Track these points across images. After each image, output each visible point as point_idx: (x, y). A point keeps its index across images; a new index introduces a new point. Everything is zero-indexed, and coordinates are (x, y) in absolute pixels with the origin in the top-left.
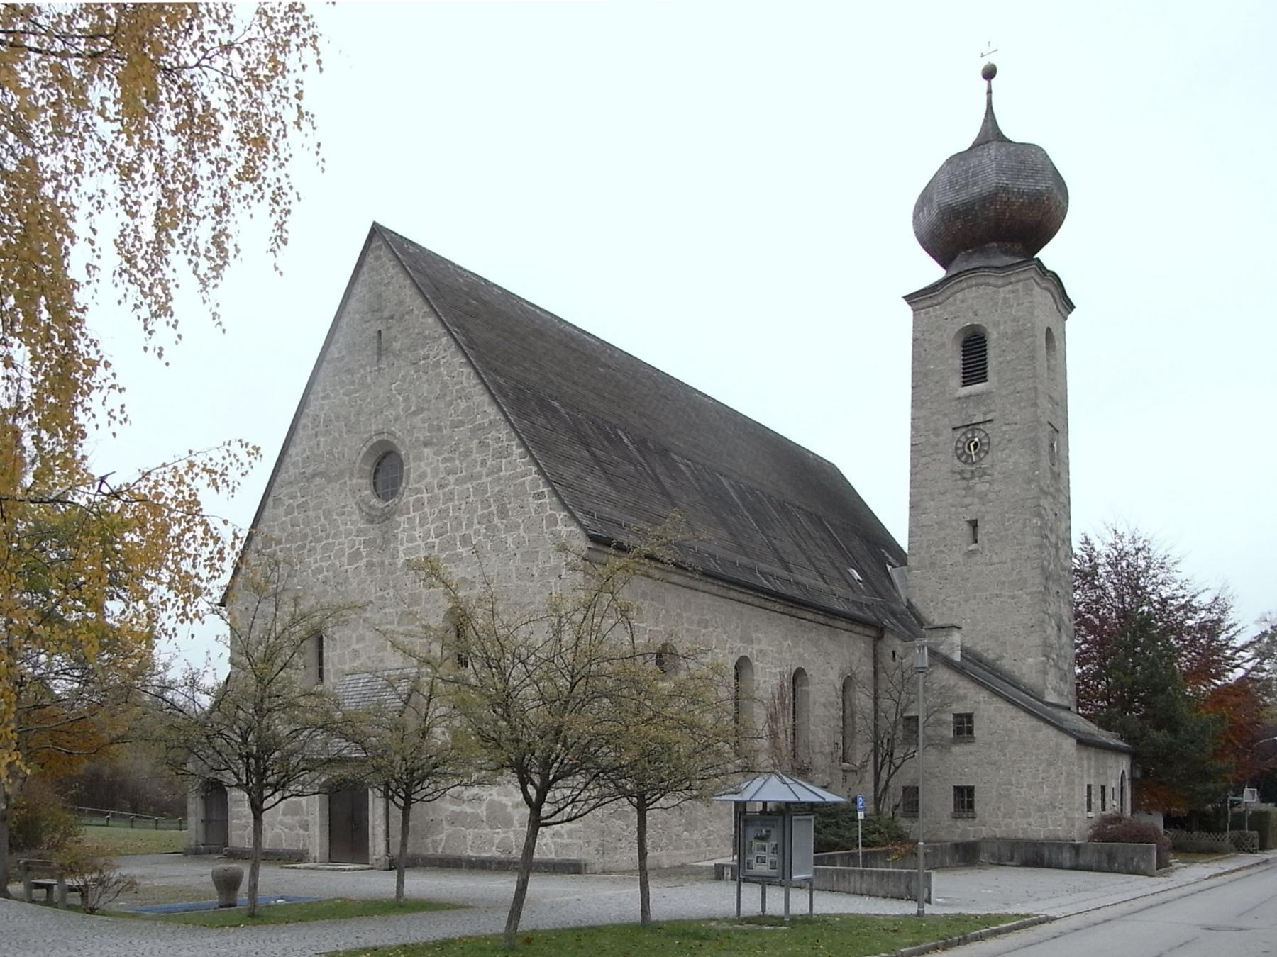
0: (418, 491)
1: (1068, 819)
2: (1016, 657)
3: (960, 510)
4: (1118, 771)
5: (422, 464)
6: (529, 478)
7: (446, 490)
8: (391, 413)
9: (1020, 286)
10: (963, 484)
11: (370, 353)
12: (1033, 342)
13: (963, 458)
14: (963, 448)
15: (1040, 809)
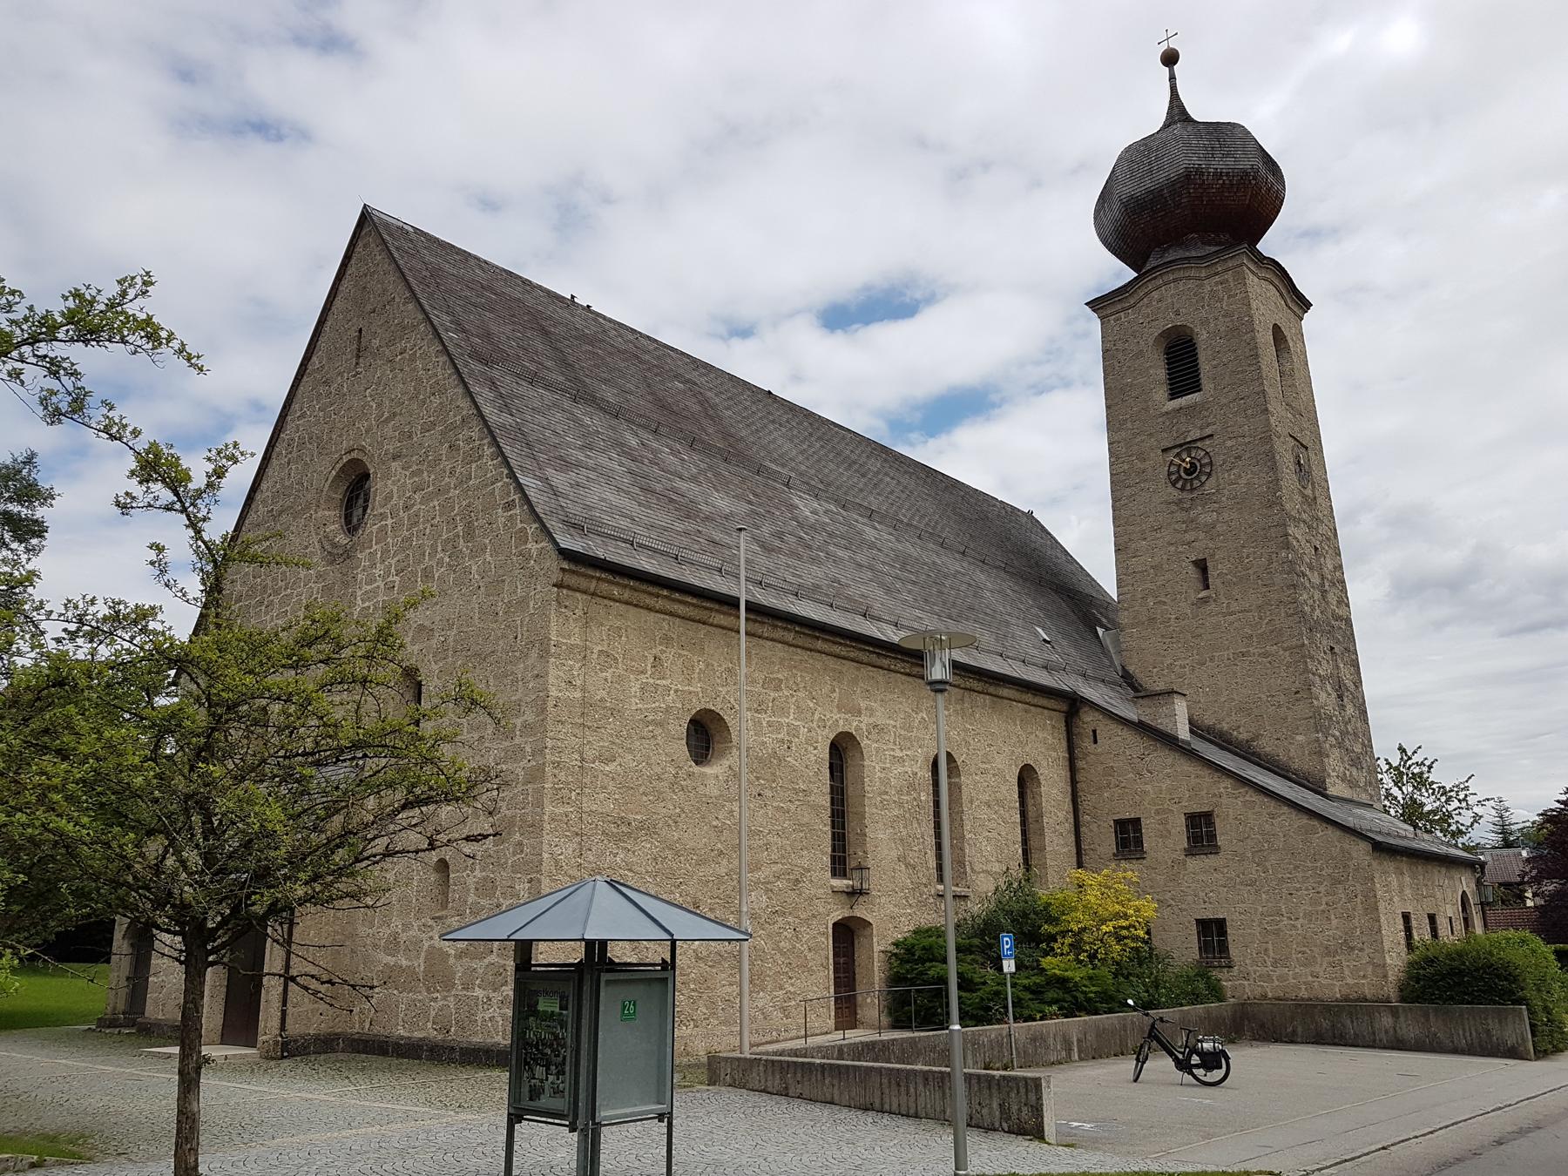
1: (1376, 966)
4: (1455, 891)
6: (499, 484)
8: (362, 425)
9: (1229, 276)
10: (1180, 516)
12: (1253, 338)
13: (1179, 485)
15: (1328, 952)
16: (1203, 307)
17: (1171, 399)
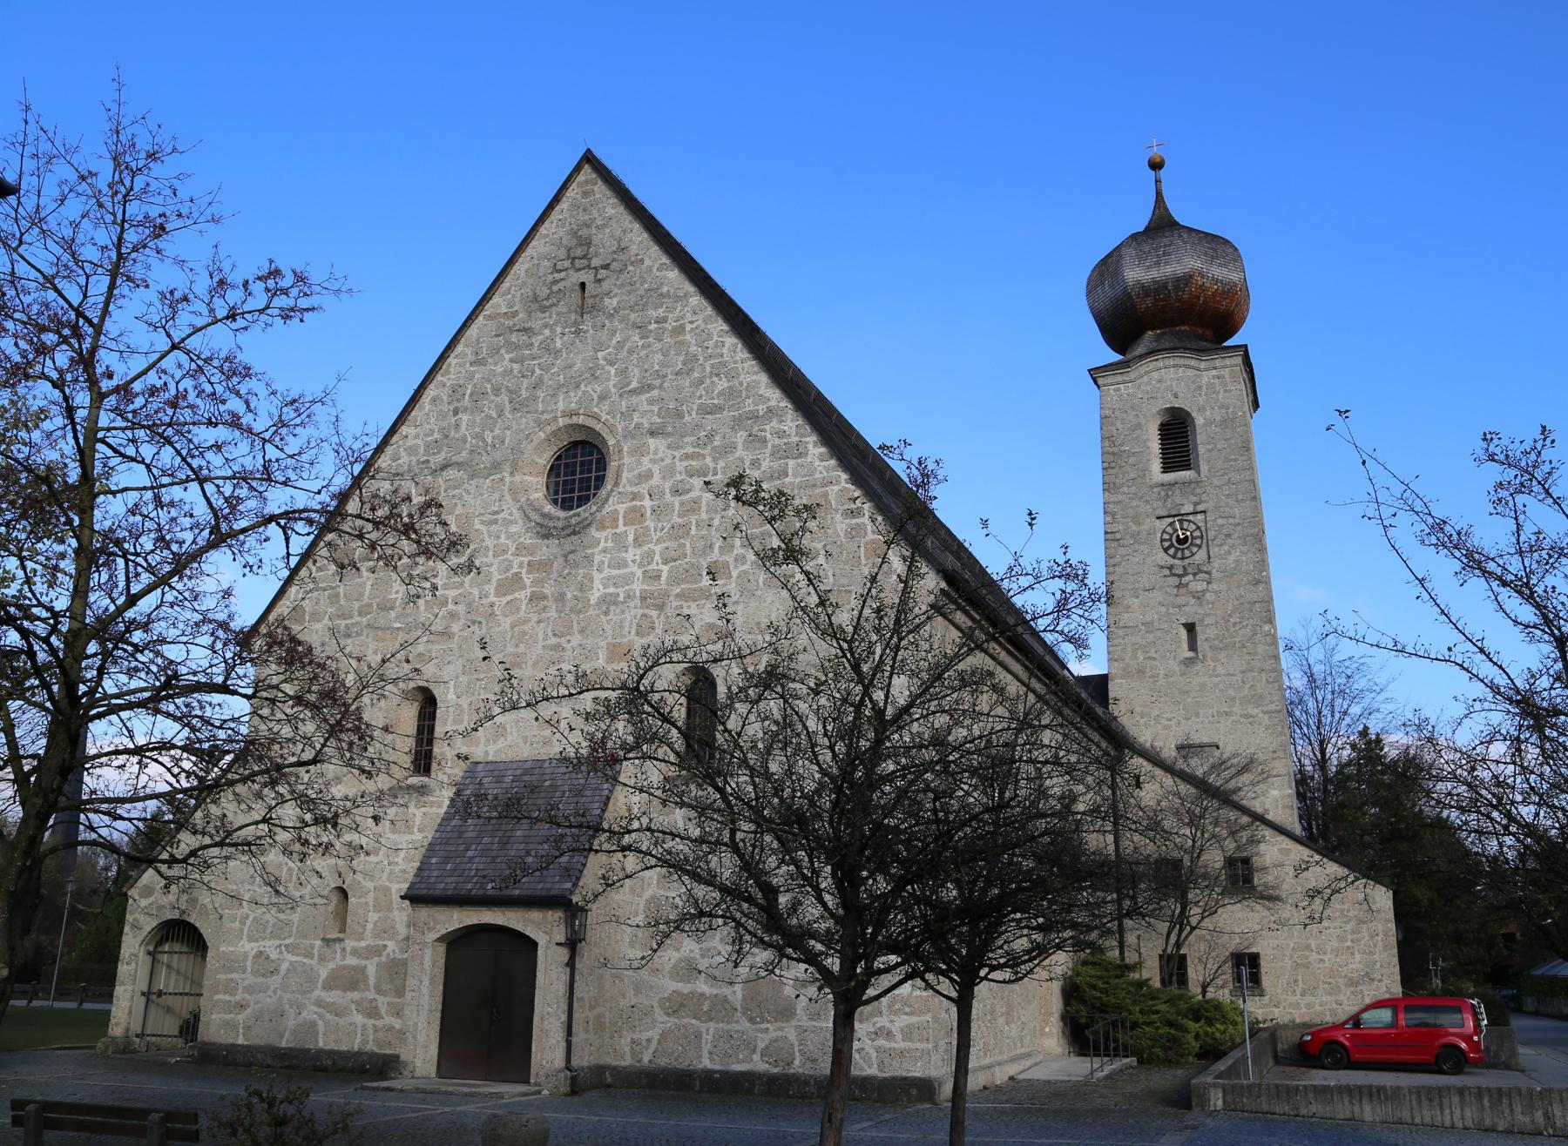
0: (635, 496)
3: (1171, 610)
5: (645, 460)
6: (836, 488)
7: (686, 497)
10: (1175, 580)
11: (564, 310)
14: (1171, 540)
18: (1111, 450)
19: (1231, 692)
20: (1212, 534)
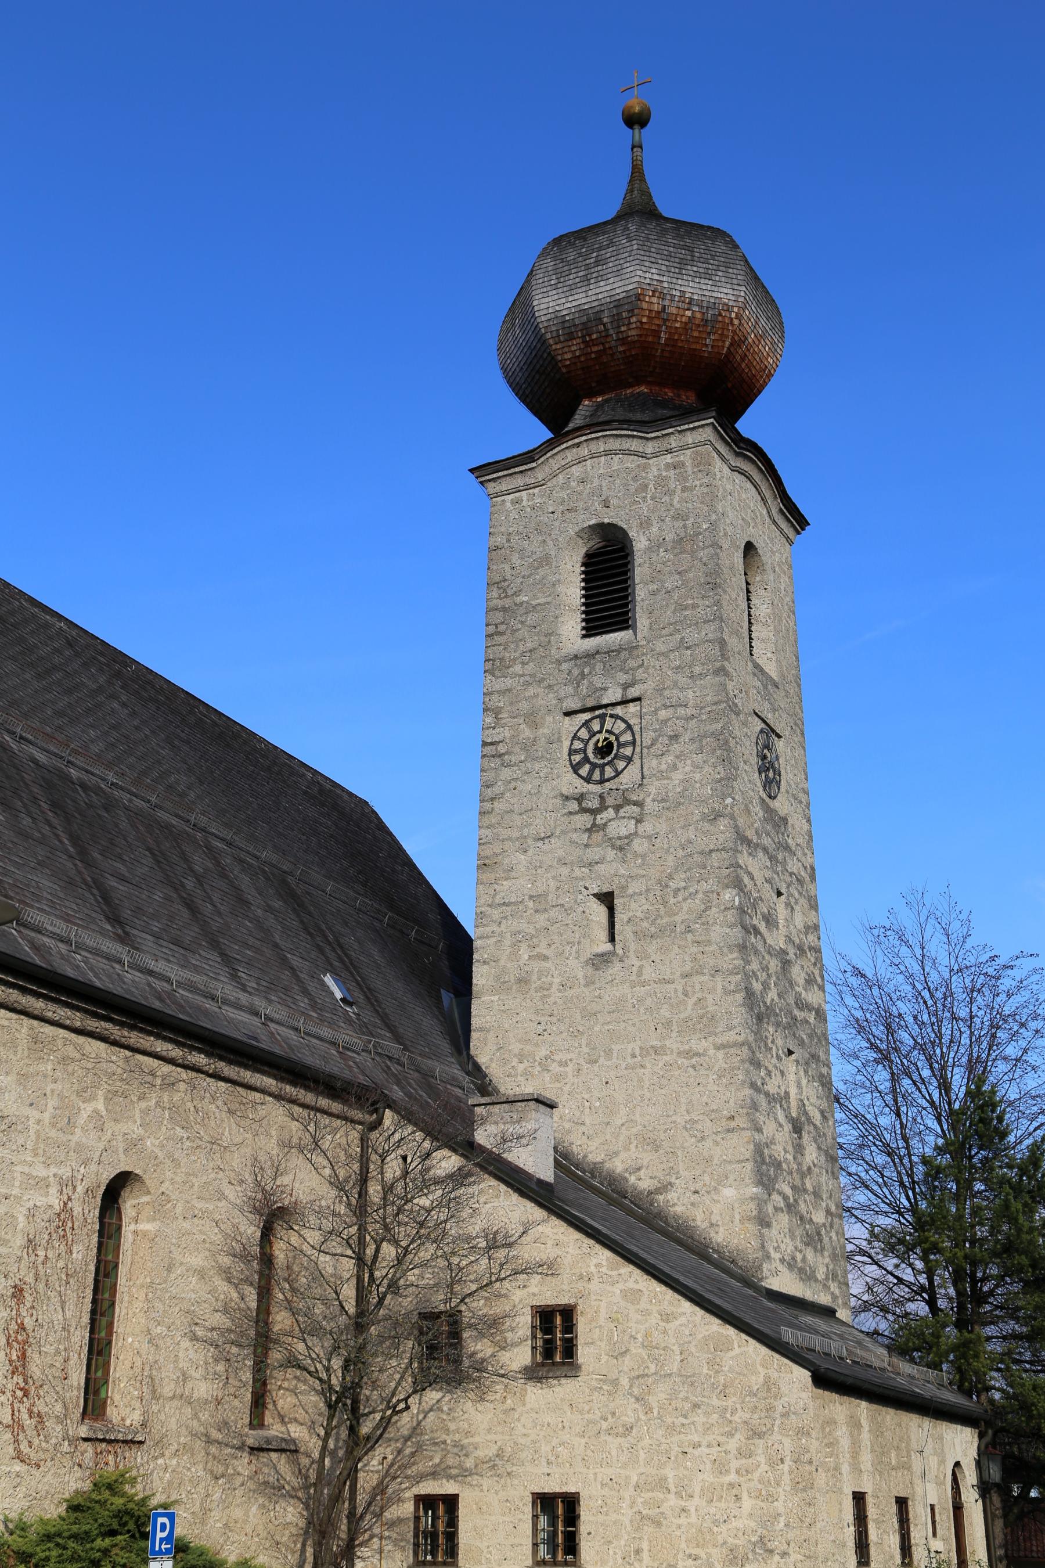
2: (698, 1186)
3: (578, 872)
4: (942, 1462)
9: (686, 457)
10: (585, 820)
13: (585, 770)
14: (585, 751)
16: (644, 498)
17: (584, 636)
18: (499, 603)
19: (665, 1012)
20: (648, 737)
